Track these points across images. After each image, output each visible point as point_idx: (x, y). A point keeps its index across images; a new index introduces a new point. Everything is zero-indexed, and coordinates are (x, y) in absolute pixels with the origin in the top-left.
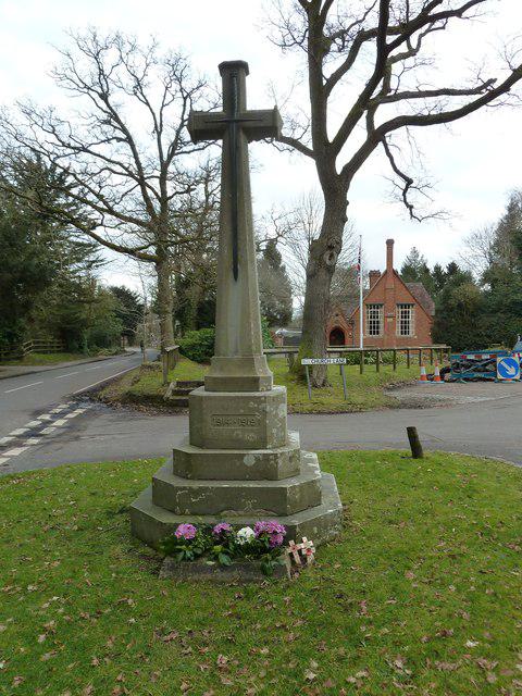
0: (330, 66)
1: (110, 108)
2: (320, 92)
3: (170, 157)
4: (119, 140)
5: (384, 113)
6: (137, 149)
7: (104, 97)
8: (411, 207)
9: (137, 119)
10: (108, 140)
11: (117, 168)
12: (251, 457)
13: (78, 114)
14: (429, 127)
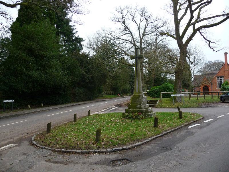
0: (179, 16)
1: (125, 25)
2: (177, 22)
3: (143, 37)
4: (128, 34)
5: (197, 26)
6: (133, 36)
7: (124, 23)
8: (212, 48)
9: (133, 27)
10: (125, 34)
11: (127, 42)
12: (139, 106)
13: (116, 28)
14: (210, 28)
